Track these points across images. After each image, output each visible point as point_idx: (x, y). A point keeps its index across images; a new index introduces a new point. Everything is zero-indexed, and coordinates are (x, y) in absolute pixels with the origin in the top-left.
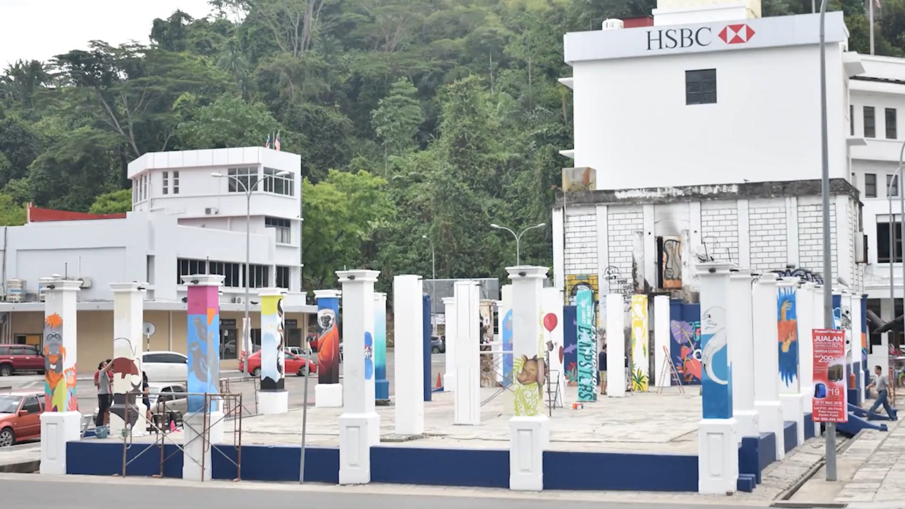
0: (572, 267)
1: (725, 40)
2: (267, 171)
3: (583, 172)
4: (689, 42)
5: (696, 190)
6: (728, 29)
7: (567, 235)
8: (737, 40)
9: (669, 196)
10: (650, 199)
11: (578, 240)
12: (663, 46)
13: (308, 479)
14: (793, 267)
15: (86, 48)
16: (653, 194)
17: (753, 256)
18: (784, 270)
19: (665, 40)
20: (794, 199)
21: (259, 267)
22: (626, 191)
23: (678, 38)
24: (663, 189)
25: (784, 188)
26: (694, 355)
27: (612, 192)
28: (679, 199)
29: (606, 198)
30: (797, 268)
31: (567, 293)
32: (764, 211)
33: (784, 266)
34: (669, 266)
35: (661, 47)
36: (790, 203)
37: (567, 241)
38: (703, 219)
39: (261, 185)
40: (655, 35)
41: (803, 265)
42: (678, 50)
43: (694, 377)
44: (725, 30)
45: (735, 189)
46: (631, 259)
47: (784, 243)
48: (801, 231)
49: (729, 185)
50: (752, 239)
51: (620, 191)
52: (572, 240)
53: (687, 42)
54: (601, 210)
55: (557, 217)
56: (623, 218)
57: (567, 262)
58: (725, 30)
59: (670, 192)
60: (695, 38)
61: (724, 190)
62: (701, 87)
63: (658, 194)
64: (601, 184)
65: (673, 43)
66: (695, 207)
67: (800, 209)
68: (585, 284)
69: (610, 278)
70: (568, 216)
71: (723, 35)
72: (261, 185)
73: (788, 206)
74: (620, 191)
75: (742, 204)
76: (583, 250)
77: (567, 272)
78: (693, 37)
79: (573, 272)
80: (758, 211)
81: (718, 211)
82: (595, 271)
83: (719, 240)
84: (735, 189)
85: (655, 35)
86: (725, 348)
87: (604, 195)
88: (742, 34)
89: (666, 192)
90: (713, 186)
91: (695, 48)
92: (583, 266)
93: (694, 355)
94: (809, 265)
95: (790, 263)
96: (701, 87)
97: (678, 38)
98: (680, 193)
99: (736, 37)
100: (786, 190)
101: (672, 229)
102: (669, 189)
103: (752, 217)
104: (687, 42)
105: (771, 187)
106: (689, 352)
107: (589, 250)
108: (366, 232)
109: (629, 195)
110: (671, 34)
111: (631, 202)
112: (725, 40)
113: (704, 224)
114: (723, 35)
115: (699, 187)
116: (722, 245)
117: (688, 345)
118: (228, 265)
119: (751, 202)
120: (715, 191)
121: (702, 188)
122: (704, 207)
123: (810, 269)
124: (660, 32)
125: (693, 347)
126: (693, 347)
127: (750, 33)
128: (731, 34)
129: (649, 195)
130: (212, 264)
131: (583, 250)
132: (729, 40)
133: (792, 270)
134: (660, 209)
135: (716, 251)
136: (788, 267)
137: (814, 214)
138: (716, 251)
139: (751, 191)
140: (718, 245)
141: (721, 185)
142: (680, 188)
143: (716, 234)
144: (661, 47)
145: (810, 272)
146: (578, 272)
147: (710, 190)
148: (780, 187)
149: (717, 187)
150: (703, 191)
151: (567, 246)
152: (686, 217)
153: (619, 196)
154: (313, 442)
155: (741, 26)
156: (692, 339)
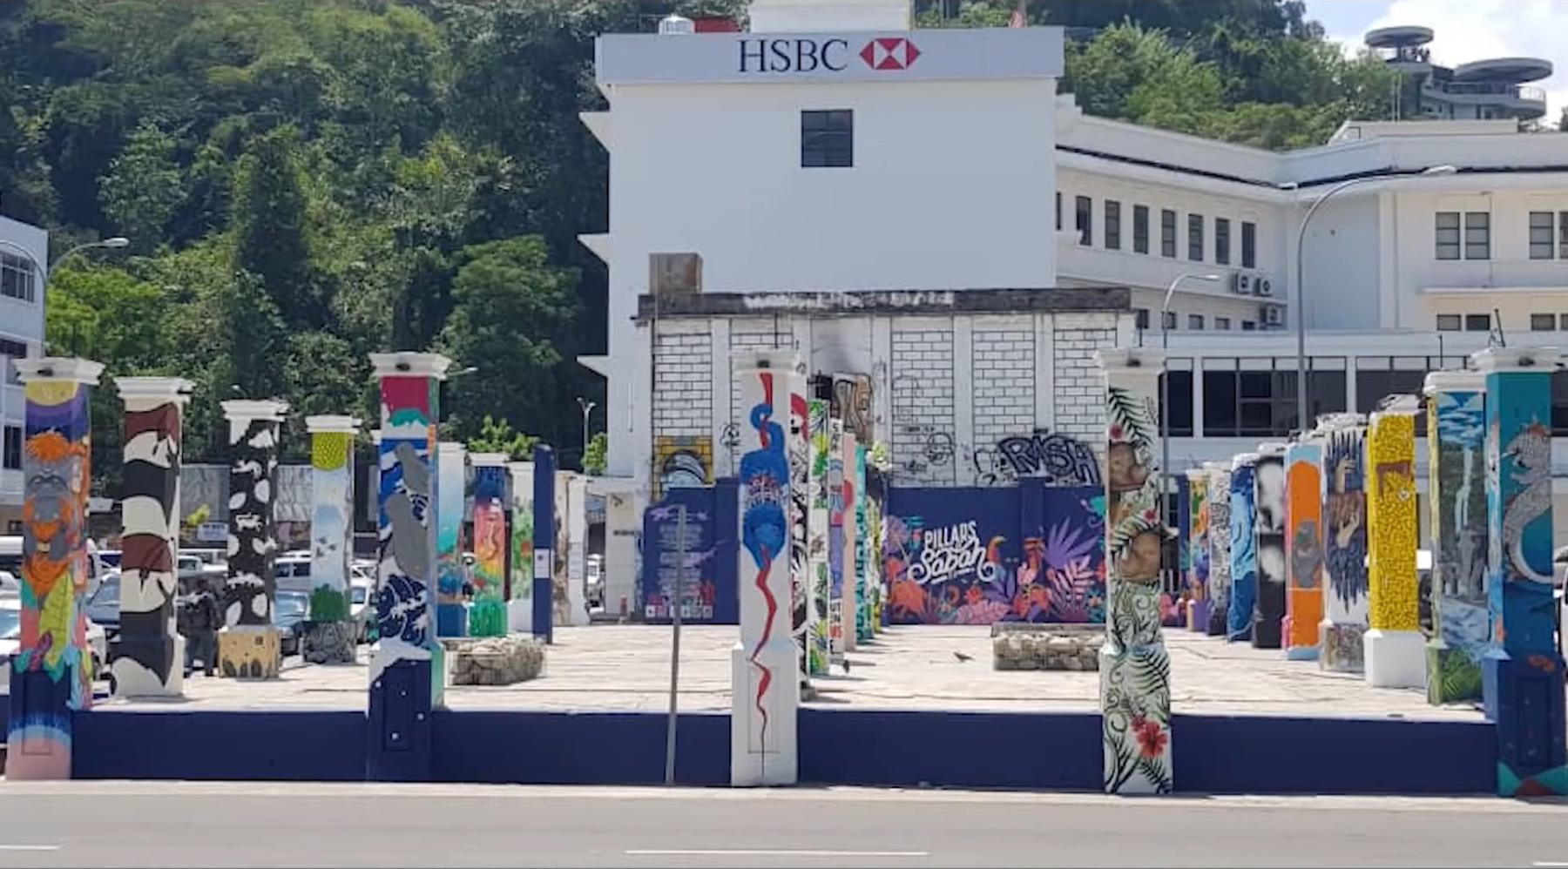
0: (666, 423)
1: (871, 62)
3: (686, 260)
4: (811, 62)
5: (883, 299)
6: (876, 45)
7: (659, 368)
10: (804, 312)
11: (677, 377)
12: (768, 67)
13: (682, 780)
14: (1046, 431)
16: (809, 303)
17: (978, 411)
18: (1030, 436)
19: (770, 56)
22: (763, 295)
23: (792, 53)
24: (827, 296)
25: (1031, 300)
26: (910, 574)
27: (740, 296)
28: (854, 311)
29: (727, 305)
30: (1052, 432)
31: (657, 469)
33: (1030, 429)
35: (763, 69)
37: (658, 377)
38: (896, 347)
40: (753, 48)
41: (1060, 429)
43: (909, 612)
44: (871, 45)
45: (948, 299)
48: (1059, 373)
51: (752, 296)
52: (666, 377)
54: (720, 326)
56: (754, 339)
57: (657, 414)
58: (871, 45)
59: (839, 300)
61: (932, 299)
62: (827, 141)
63: (819, 303)
64: (709, 285)
65: (784, 64)
66: (882, 324)
68: (689, 452)
70: (660, 336)
71: (868, 54)
75: (962, 323)
76: (686, 395)
77: (658, 432)
78: (818, 55)
79: (666, 432)
82: (707, 432)
84: (948, 299)
85: (753, 48)
86: (1550, 509)
87: (725, 302)
89: (832, 300)
90: (913, 292)
92: (687, 423)
93: (910, 574)
94: (1071, 429)
95: (1040, 425)
96: (827, 141)
97: (792, 53)
98: (856, 302)
99: (888, 55)
100: (1035, 304)
101: (841, 362)
102: (836, 295)
103: (976, 346)
105: (1009, 297)
106: (900, 567)
107: (695, 395)
109: (769, 302)
110: (780, 47)
112: (871, 62)
114: (868, 54)
115: (889, 293)
116: (927, 392)
117: (899, 556)
121: (894, 296)
123: (1071, 436)
124: (762, 43)
125: (907, 559)
126: (907, 559)
129: (801, 304)
131: (686, 395)
132: (877, 62)
133: (1043, 437)
135: (917, 402)
137: (667, 405)
138: (917, 402)
139: (973, 302)
140: (919, 393)
141: (926, 293)
142: (856, 294)
143: (918, 374)
144: (763, 69)
146: (676, 433)
147: (907, 299)
148: (1026, 298)
149: (919, 295)
151: (658, 386)
152: (865, 343)
153: (750, 303)
154: (689, 705)
155: (898, 41)
156: (906, 546)
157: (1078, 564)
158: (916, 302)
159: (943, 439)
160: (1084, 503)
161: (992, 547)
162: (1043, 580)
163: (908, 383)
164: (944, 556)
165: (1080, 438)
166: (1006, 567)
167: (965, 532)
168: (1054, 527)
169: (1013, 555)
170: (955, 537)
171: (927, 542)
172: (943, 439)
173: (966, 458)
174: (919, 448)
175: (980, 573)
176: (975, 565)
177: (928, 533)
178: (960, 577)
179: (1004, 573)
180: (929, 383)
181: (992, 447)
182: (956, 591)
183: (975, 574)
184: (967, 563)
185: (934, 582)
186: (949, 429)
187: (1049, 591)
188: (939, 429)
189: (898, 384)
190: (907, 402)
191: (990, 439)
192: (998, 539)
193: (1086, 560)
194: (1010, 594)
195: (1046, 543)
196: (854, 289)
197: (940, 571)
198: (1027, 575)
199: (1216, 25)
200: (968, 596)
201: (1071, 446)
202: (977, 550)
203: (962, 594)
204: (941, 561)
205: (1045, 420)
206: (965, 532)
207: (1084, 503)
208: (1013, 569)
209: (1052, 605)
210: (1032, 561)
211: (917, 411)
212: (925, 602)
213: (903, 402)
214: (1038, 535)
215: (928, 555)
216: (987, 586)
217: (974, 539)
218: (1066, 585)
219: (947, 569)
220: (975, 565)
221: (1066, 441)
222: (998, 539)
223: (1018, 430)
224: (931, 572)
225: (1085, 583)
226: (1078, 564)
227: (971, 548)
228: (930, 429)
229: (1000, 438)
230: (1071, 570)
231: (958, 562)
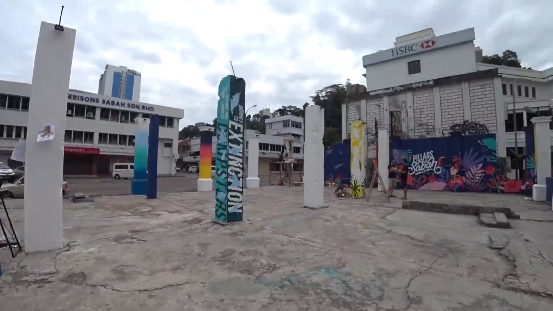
2: (292, 121)
5: (410, 86)
8: (428, 46)
9: (396, 91)
14: (467, 121)
15: (282, 108)
16: (388, 91)
20: (467, 84)
21: (264, 144)
22: (375, 91)
24: (393, 88)
28: (401, 92)
30: (470, 122)
32: (449, 92)
33: (462, 121)
34: (396, 124)
36: (465, 86)
38: (415, 100)
39: (290, 125)
41: (473, 120)
42: (404, 54)
46: (374, 121)
47: (472, 95)
49: (428, 81)
50: (442, 108)
51: (372, 92)
53: (407, 51)
54: (363, 103)
55: (344, 107)
56: (373, 104)
60: (411, 48)
61: (425, 84)
63: (391, 91)
67: (471, 88)
69: (368, 133)
71: (422, 46)
72: (290, 125)
73: (463, 88)
74: (372, 92)
80: (445, 92)
81: (423, 97)
83: (423, 110)
88: (430, 44)
89: (395, 89)
90: (419, 83)
91: (411, 52)
94: (478, 120)
95: (466, 119)
98: (402, 88)
104: (407, 51)
108: (500, 190)
111: (378, 97)
113: (415, 103)
114: (422, 46)
115: (411, 84)
118: (277, 146)
119: (441, 90)
120: (421, 85)
122: (415, 93)
127: (433, 43)
128: (425, 45)
130: (272, 145)
134: (392, 98)
135: (422, 116)
136: (464, 122)
141: (424, 82)
142: (402, 86)
143: (422, 107)
145: (478, 124)
147: (417, 85)
150: (414, 86)
157: (477, 167)
158: (421, 85)
159: (431, 127)
160: (479, 141)
161: (440, 160)
162: (462, 173)
163: (419, 110)
164: (420, 164)
165: (481, 123)
166: (445, 168)
167: (429, 155)
168: (466, 153)
169: (446, 164)
170: (425, 157)
171: (414, 159)
172: (431, 127)
173: (439, 133)
174: (423, 130)
175: (434, 170)
176: (433, 168)
177: (414, 156)
178: (427, 172)
179: (444, 170)
180: (426, 110)
181: (448, 128)
182: (425, 178)
183: (432, 171)
184: (430, 166)
185: (416, 174)
186: (433, 124)
187: (463, 178)
188: (430, 124)
189: (416, 111)
190: (419, 116)
191: (448, 125)
192: (442, 157)
193: (481, 166)
194: (447, 178)
195: (463, 159)
196: (401, 85)
197: (419, 170)
198: (454, 172)
199: (502, 153)
200: (430, 179)
201: (478, 126)
202: (433, 162)
203: (428, 178)
204: (419, 166)
205: (468, 118)
206: (429, 155)
207: (479, 141)
208: (448, 169)
209: (465, 184)
210: (456, 165)
211: (422, 119)
212: (413, 181)
213: (417, 116)
214: (458, 155)
215: (414, 164)
216: (437, 176)
217: (432, 157)
218: (472, 176)
219: (422, 169)
220: (433, 168)
221: (476, 124)
222: (442, 157)
223: (458, 122)
224: (416, 170)
225: (480, 175)
226: (477, 167)
227: (431, 161)
228: (427, 124)
229: (451, 125)
230: (474, 170)
231: (426, 166)
